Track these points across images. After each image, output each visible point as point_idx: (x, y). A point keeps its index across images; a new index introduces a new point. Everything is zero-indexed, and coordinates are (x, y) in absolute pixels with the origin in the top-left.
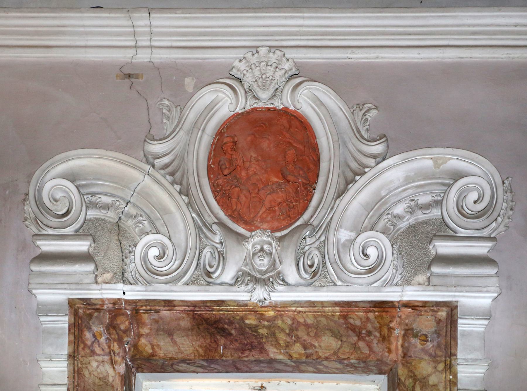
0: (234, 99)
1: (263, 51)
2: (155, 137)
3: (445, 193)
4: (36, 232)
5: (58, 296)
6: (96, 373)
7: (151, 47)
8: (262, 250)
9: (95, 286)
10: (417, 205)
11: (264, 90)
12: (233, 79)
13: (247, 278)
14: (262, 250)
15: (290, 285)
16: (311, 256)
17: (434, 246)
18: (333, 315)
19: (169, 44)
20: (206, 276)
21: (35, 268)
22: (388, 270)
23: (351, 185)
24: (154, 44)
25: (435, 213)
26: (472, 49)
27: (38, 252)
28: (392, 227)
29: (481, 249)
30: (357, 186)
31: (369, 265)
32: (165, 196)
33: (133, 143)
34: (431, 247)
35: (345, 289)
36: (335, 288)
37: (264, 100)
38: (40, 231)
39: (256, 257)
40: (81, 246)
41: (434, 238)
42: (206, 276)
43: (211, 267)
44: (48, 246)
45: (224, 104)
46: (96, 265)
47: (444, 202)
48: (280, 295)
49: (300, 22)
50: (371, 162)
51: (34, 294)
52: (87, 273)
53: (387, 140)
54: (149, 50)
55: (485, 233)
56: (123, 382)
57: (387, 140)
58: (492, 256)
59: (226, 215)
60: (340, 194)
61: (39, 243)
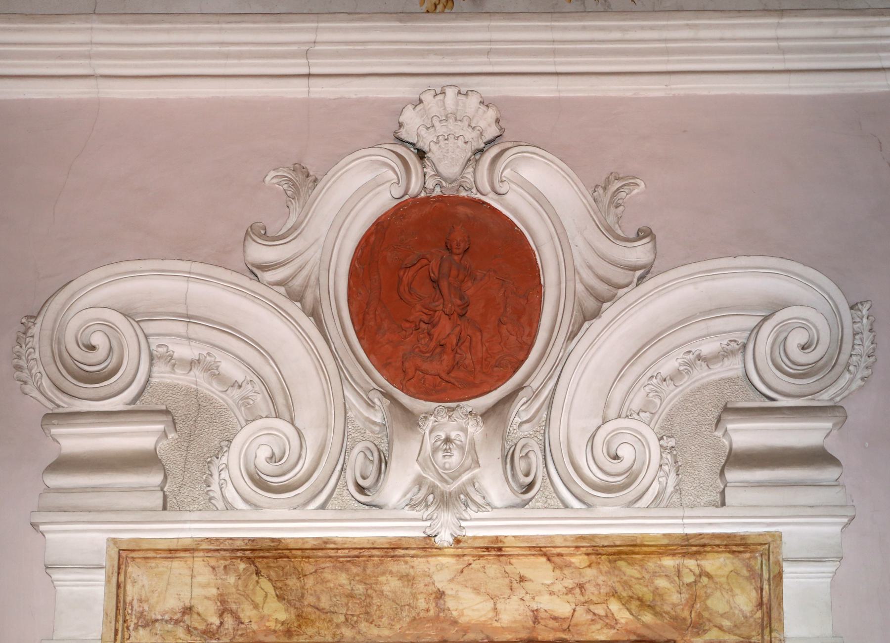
0: (404, 176)
2: (269, 234)
10: (699, 357)
15: (496, 508)
16: (527, 451)
19: (346, 222)
22: (656, 478)
23: (609, 304)
30: (618, 306)
33: (234, 243)
36: (229, 515)
40: (140, 437)
41: (725, 417)
43: (364, 478)
44: (75, 440)
46: (166, 477)
47: (750, 346)
51: (42, 533)
55: (824, 399)
60: (572, 336)
61: (54, 431)
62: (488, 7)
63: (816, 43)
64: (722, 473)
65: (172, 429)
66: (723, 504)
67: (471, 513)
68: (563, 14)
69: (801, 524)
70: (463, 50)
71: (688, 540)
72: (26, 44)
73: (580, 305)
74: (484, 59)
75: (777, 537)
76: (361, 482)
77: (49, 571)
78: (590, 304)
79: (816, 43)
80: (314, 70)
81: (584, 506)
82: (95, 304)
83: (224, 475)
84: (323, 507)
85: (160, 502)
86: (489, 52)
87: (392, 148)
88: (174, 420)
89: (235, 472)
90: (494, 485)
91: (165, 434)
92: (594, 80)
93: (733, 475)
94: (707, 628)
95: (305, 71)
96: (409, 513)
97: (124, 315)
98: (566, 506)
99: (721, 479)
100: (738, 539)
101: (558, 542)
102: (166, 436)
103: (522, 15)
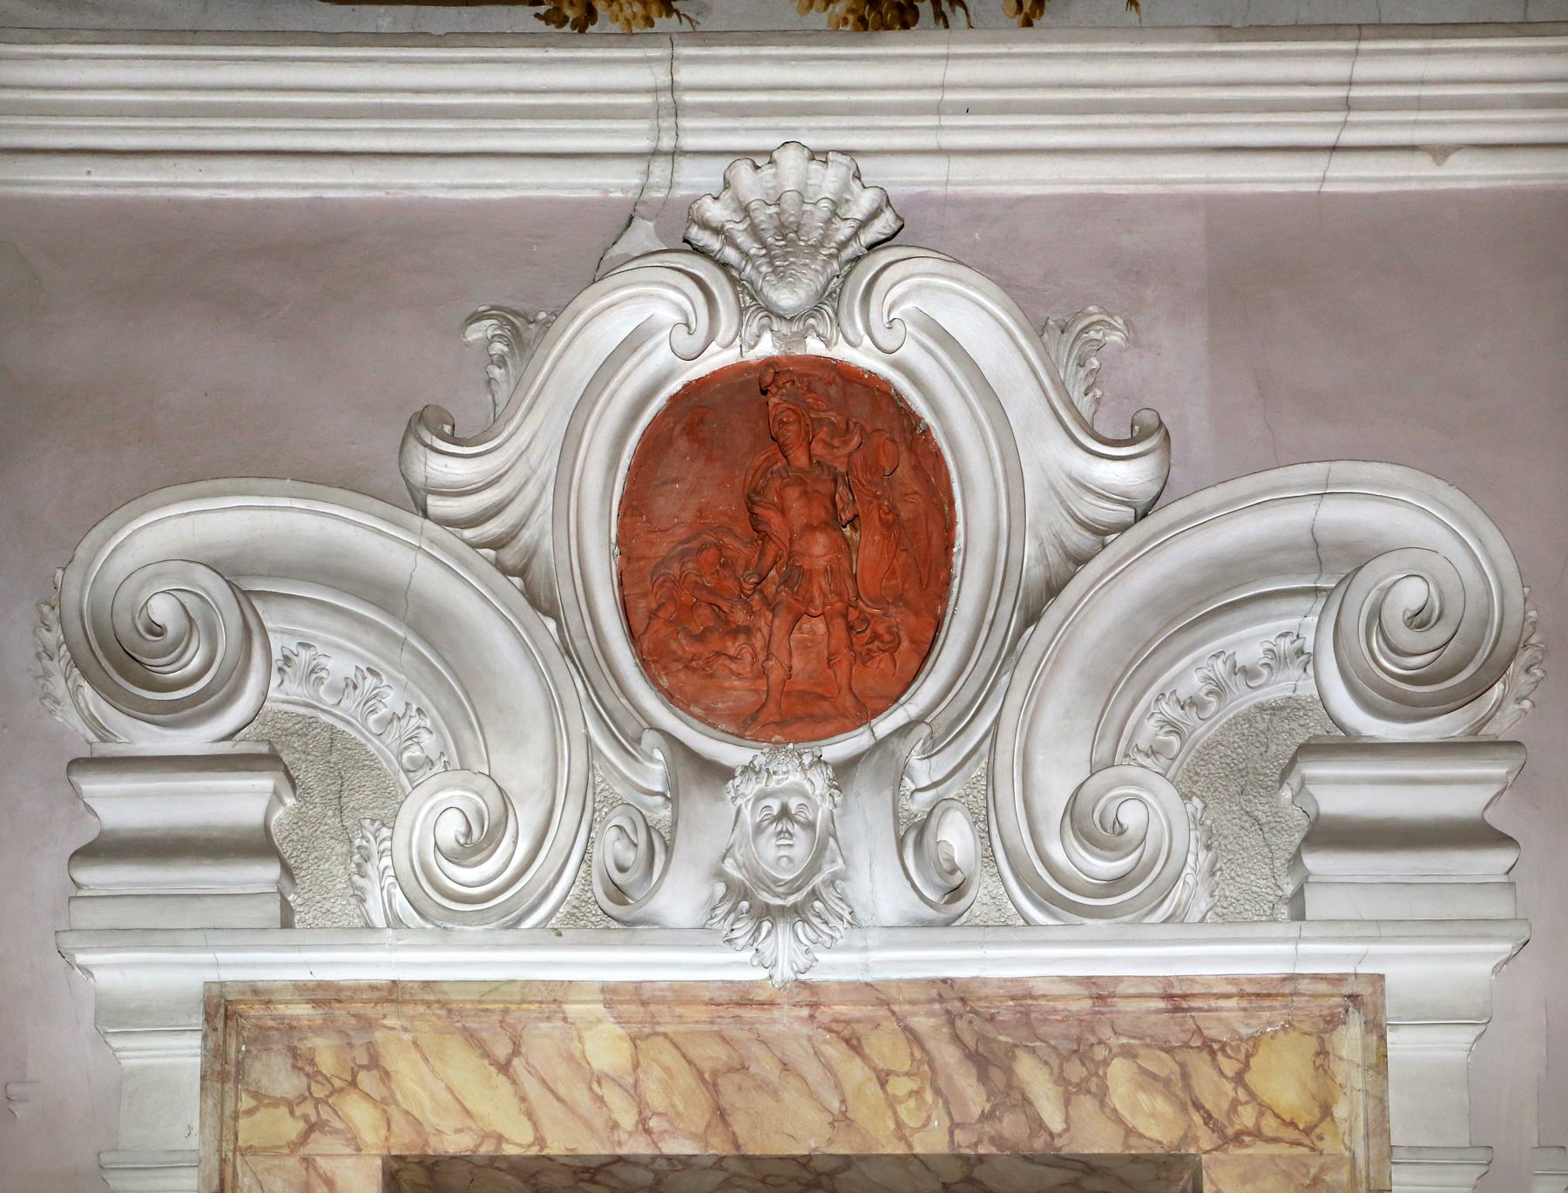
1: (791, 161)
5: (177, 973)
7: (675, 153)
8: (785, 813)
12: (686, 251)
13: (752, 904)
14: (785, 813)
20: (619, 906)
24: (689, 142)
26: (1388, 154)
27: (87, 835)
28: (1174, 739)
29: (1457, 792)
34: (1286, 794)
35: (1061, 934)
36: (1030, 934)
39: (763, 839)
40: (242, 800)
43: (622, 869)
44: (121, 804)
45: (654, 333)
46: (287, 870)
48: (839, 963)
49: (935, 73)
54: (640, 166)
56: (1249, 989)
58: (1496, 819)
62: (706, 25)
65: (288, 786)
69: (1429, 963)
73: (1062, 544)
76: (618, 878)
78: (1080, 540)
80: (1350, 137)
83: (387, 861)
86: (938, 109)
90: (880, 885)
91: (277, 795)
93: (1315, 862)
94: (419, 1171)
95: (1327, 137)
98: (1028, 922)
100: (516, 989)
101: (1042, 988)
102: (281, 801)
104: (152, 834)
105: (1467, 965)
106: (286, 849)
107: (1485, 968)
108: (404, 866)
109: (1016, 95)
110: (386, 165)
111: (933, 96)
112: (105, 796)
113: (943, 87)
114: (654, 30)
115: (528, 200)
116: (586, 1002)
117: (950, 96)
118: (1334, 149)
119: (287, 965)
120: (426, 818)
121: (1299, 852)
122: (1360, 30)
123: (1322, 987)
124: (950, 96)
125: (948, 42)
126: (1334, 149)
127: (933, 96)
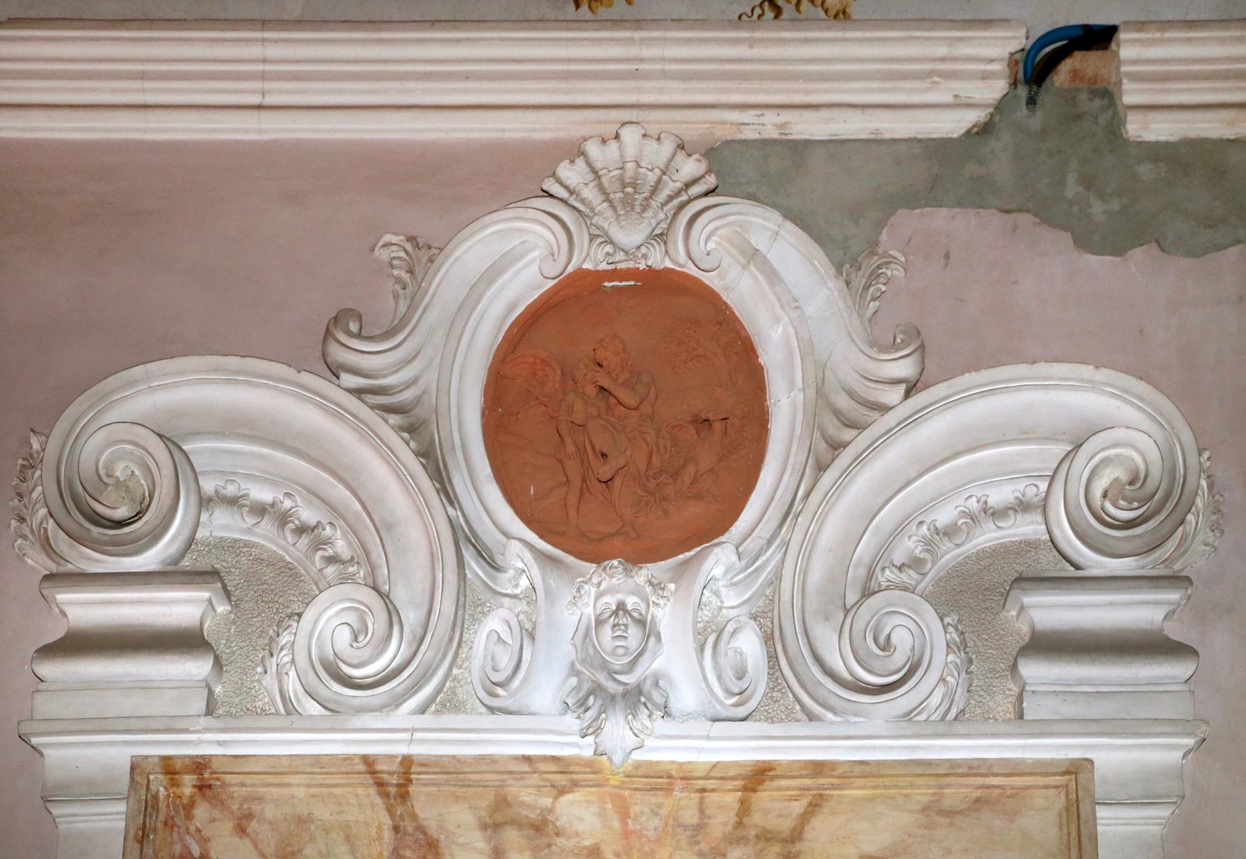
3: (1052, 478)
4: (53, 567)
6: (506, 605)
9: (204, 721)
11: (628, 203)
17: (1022, 608)
18: (821, 795)
21: (51, 670)
25: (1028, 528)
31: (902, 663)
32: (385, 471)
33: (322, 341)
37: (630, 242)
38: (59, 564)
40: (179, 607)
42: (497, 695)
44: (85, 608)
46: (218, 664)
50: (893, 395)
52: (182, 686)
53: (922, 347)
57: (922, 347)
58: (1175, 632)
59: (1114, 242)
63: (728, 67)
64: (1014, 668)
66: (1021, 716)
67: (660, 726)
68: (541, 22)
70: (277, 72)
71: (569, 765)
72: (348, 61)
74: (137, 84)
75: (1091, 762)
77: (49, 805)
79: (713, 67)
80: (270, 100)
81: (328, 713)
82: (118, 423)
84: (422, 710)
85: (202, 705)
87: (549, 209)
88: (224, 587)
89: (302, 661)
92: (194, 115)
95: (255, 99)
96: (705, 727)
97: (160, 436)
98: (812, 717)
99: (1013, 677)
103: (137, 23)
104: (1132, 631)
105: (1162, 753)
106: (221, 647)
107: (1178, 755)
108: (302, 661)
109: (811, 67)
110: (93, 114)
111: (259, 67)
112: (70, 603)
113: (264, 61)
114: (800, 17)
115: (238, 142)
116: (435, 773)
117: (269, 67)
118: (259, 107)
119: (246, 742)
120: (329, 620)
121: (1016, 660)
122: (264, 24)
123: (553, 767)
124: (269, 67)
125: (844, 29)
126: (259, 107)
127: (259, 67)
